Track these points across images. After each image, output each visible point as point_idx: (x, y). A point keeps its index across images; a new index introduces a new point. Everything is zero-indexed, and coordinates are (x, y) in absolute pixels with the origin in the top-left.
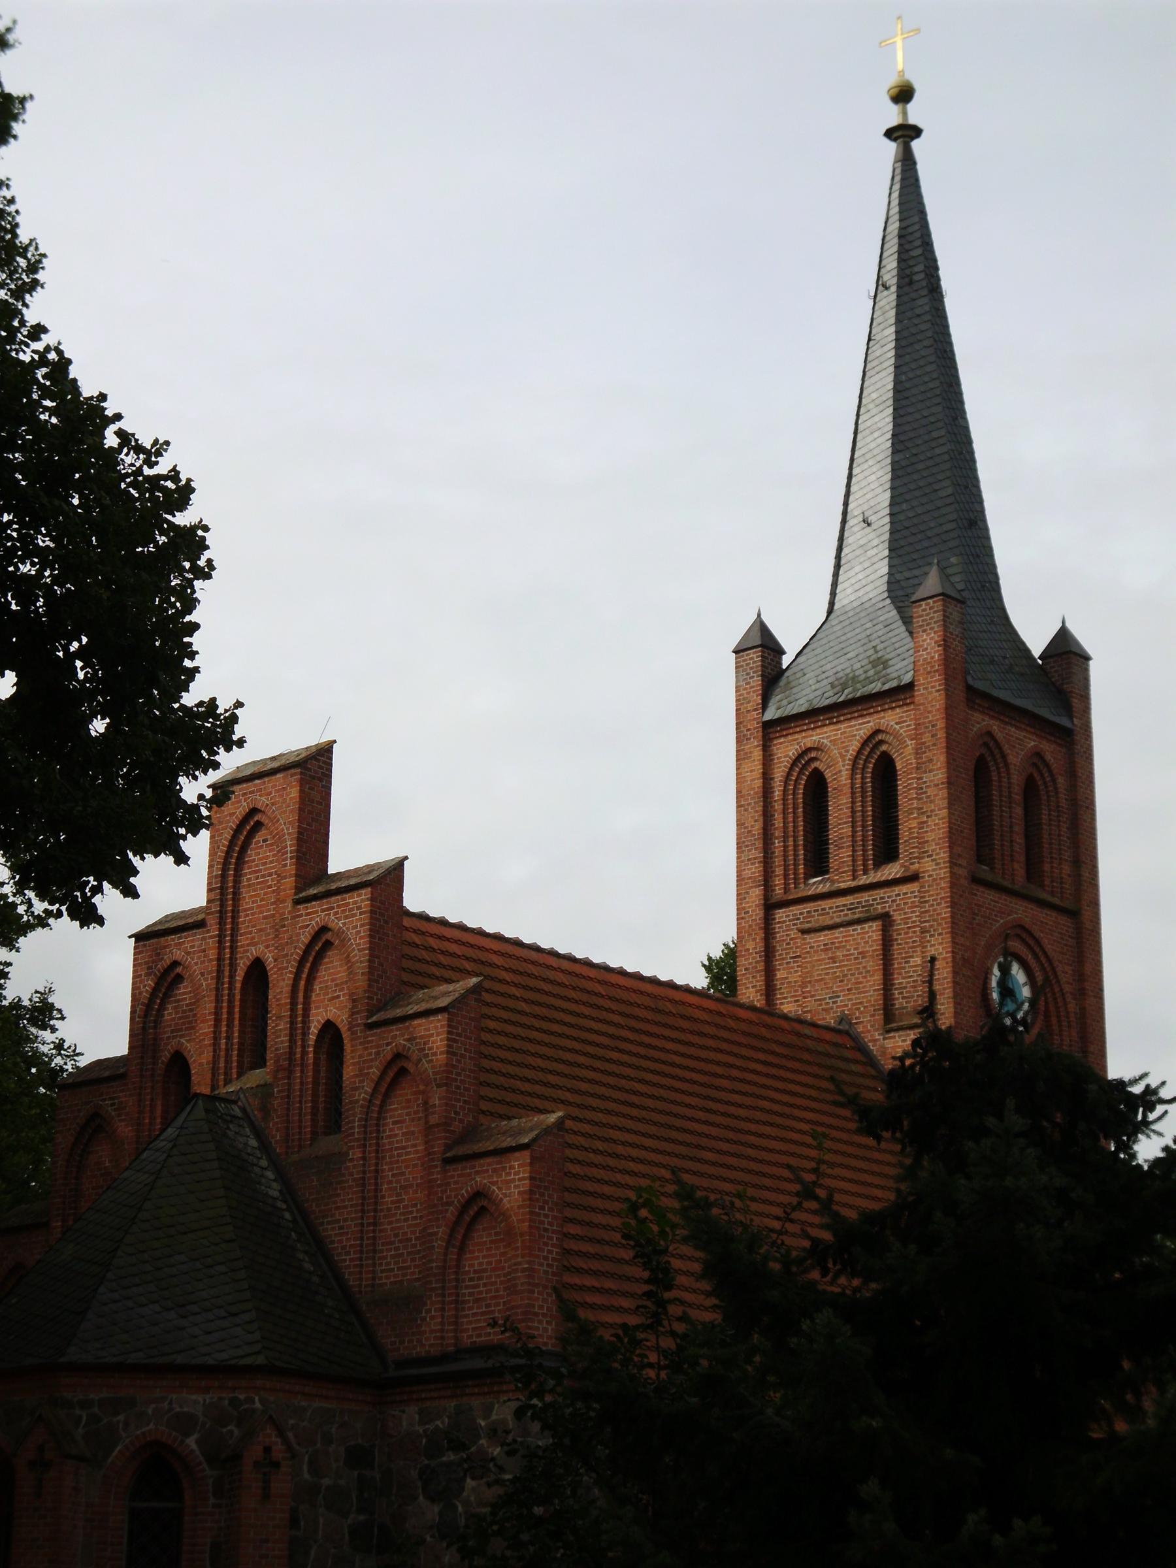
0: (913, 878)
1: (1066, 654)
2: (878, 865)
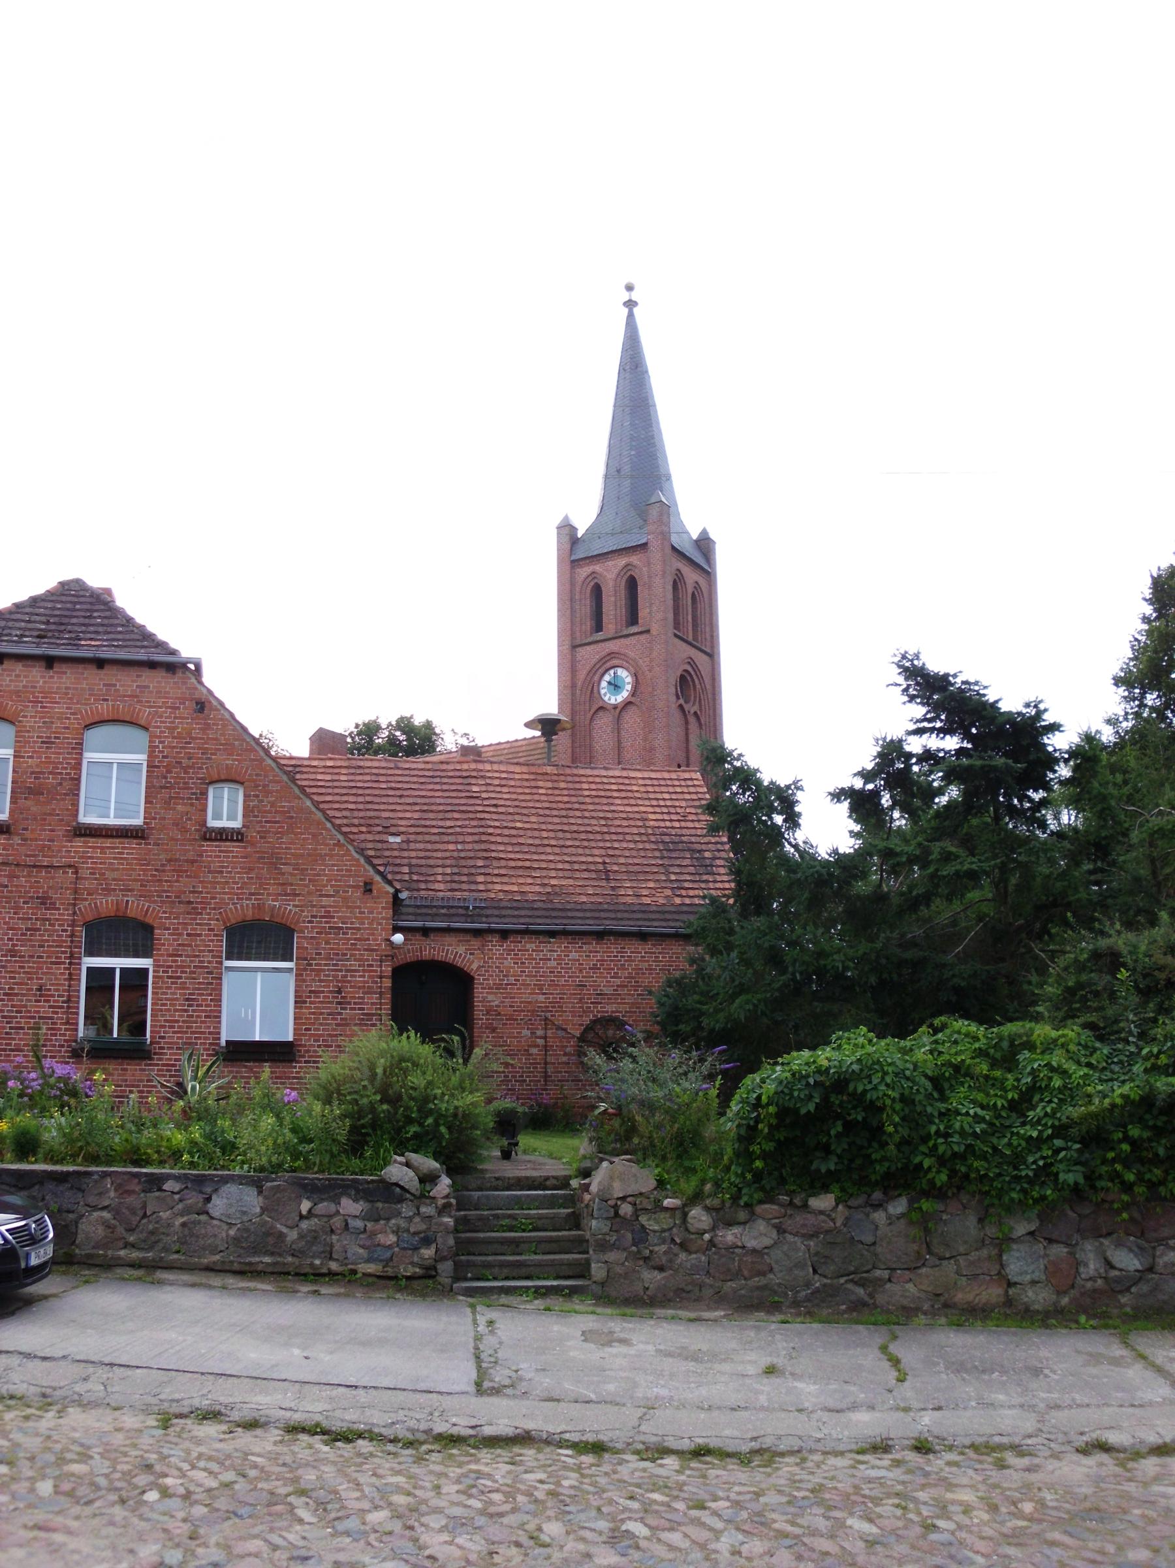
0: (648, 631)
1: (705, 544)
2: (627, 626)
